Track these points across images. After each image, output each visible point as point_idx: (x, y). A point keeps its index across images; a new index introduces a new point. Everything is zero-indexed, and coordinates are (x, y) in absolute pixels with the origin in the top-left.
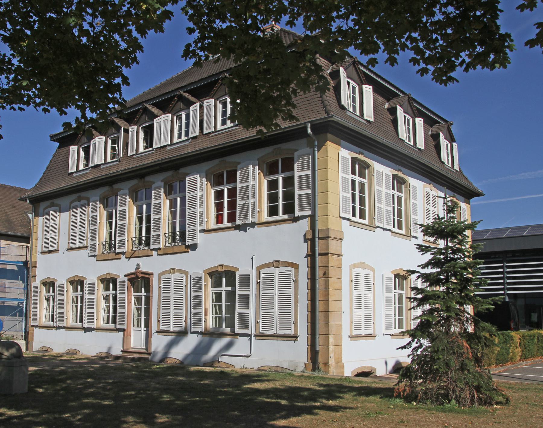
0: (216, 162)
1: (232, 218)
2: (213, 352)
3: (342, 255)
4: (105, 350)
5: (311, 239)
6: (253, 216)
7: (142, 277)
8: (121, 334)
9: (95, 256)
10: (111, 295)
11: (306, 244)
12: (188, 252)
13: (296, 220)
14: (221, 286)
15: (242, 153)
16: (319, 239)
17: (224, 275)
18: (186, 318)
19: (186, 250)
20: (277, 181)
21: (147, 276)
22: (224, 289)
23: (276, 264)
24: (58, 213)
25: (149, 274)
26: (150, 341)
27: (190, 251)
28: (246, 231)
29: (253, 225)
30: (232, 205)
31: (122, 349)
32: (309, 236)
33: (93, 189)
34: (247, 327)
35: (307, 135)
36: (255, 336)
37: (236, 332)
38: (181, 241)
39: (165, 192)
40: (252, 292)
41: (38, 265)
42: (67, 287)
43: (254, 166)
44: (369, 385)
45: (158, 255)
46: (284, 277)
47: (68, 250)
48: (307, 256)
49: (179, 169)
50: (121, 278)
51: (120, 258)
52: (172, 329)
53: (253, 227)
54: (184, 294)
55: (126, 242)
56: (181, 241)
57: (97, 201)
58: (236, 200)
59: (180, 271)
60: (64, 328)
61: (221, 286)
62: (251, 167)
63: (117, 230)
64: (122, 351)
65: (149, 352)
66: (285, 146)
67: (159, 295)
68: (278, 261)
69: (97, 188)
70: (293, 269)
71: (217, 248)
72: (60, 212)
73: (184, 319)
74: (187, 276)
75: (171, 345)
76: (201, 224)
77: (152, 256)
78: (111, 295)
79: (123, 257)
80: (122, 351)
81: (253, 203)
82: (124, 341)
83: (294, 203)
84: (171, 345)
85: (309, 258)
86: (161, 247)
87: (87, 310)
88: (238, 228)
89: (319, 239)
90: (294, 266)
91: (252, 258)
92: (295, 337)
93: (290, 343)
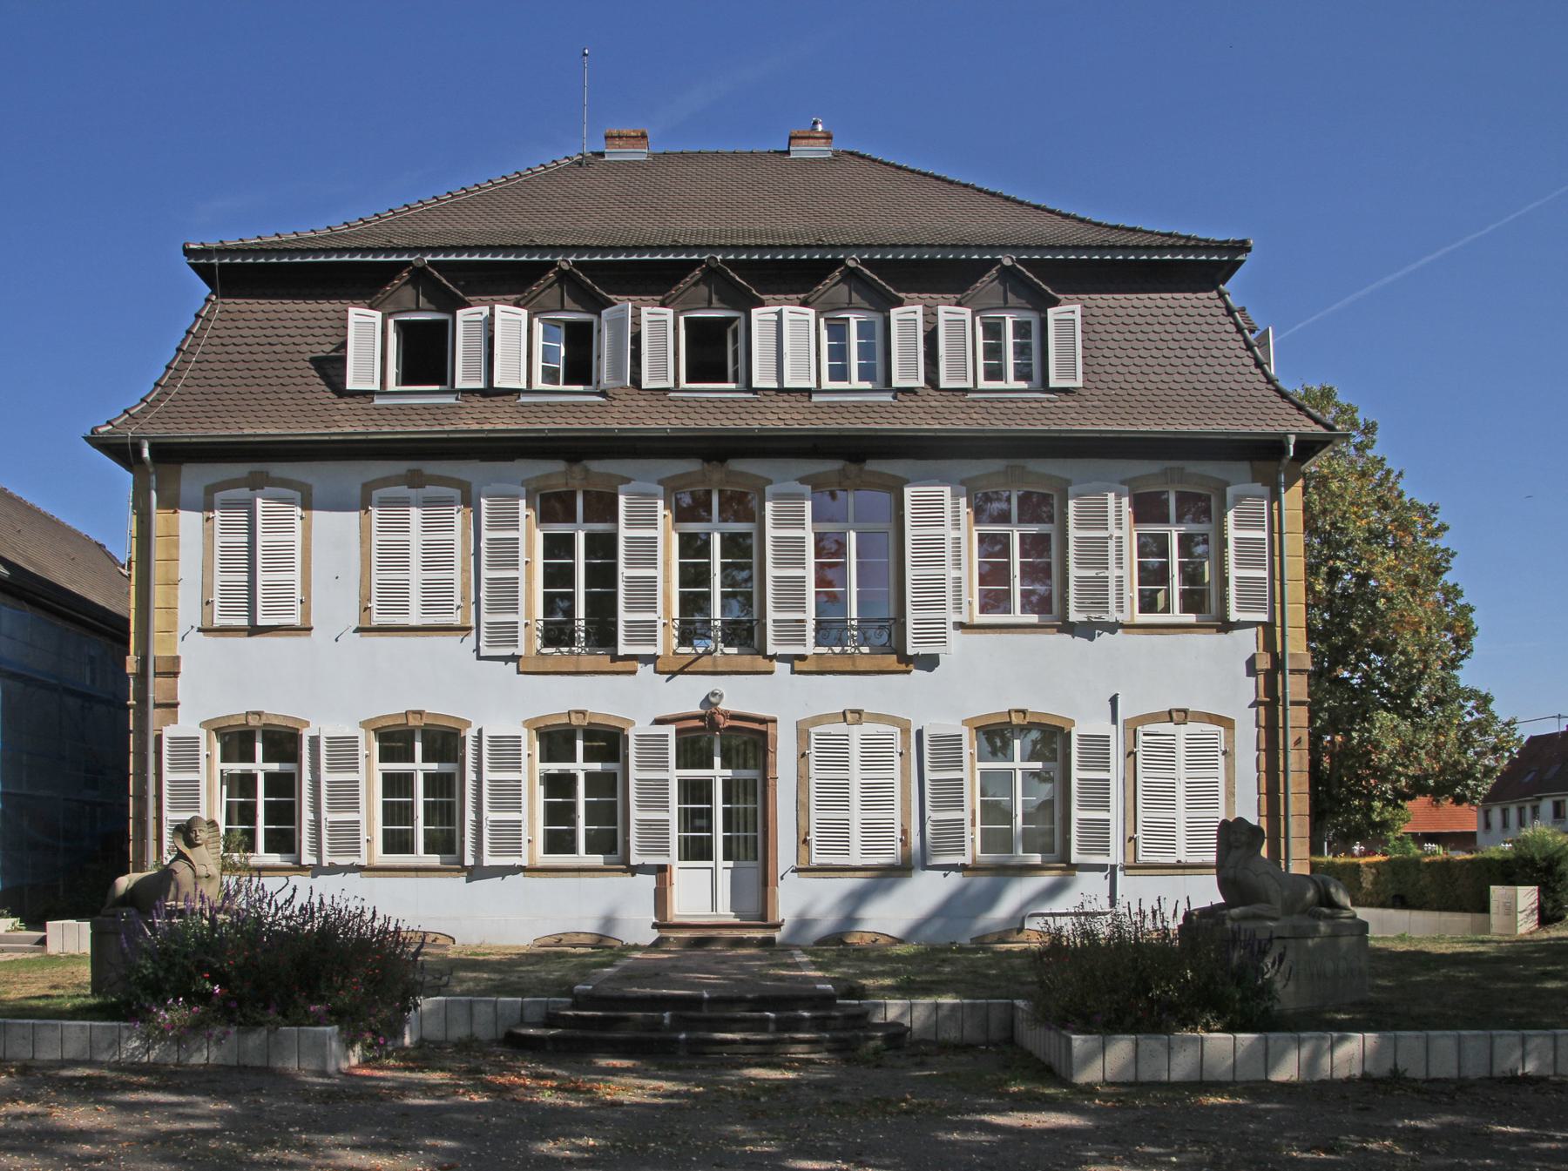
0: (997, 465)
1: (1192, 601)
2: (1005, 908)
3: (176, 705)
4: (590, 926)
5: (1267, 671)
6: (1120, 608)
7: (730, 728)
8: (650, 881)
9: (514, 658)
10: (1019, 773)
11: (1253, 679)
12: (908, 672)
13: (1226, 626)
14: (253, 760)
16: (156, 674)
18: (904, 832)
19: (903, 667)
20: (570, 539)
21: (762, 728)
22: (419, 767)
23: (1180, 716)
24: (298, 511)
25: (763, 721)
26: (774, 892)
27: (915, 672)
28: (1091, 639)
29: (1113, 628)
30: (603, 575)
32: (1264, 663)
33: (483, 459)
34: (1105, 850)
36: (1125, 868)
38: (890, 644)
40: (1115, 774)
41: (182, 669)
42: (209, 746)
43: (1119, 496)
44: (1420, 947)
45: (793, 672)
47: (358, 630)
48: (1256, 704)
49: (864, 461)
50: (639, 727)
51: (634, 673)
52: (856, 859)
54: (896, 774)
55: (660, 628)
56: (890, 644)
57: (517, 497)
58: (614, 567)
59: (878, 718)
60: (522, 869)
61: (253, 760)
62: (1111, 496)
63: (483, 595)
65: (770, 922)
66: (596, 466)
67: (802, 779)
68: (1185, 711)
69: (512, 459)
71: (983, 670)
72: (304, 508)
73: (898, 835)
74: (905, 731)
75: (859, 898)
76: (958, 608)
77: (771, 673)
78: (1019, 773)
79: (645, 671)
80: (655, 926)
81: (1120, 579)
82: (661, 898)
83: (614, 596)
84: (859, 898)
85: (1262, 709)
86: (660, 652)
87: (522, 817)
88: (1068, 628)
89: (156, 674)
90: (1227, 723)
91: (1114, 701)
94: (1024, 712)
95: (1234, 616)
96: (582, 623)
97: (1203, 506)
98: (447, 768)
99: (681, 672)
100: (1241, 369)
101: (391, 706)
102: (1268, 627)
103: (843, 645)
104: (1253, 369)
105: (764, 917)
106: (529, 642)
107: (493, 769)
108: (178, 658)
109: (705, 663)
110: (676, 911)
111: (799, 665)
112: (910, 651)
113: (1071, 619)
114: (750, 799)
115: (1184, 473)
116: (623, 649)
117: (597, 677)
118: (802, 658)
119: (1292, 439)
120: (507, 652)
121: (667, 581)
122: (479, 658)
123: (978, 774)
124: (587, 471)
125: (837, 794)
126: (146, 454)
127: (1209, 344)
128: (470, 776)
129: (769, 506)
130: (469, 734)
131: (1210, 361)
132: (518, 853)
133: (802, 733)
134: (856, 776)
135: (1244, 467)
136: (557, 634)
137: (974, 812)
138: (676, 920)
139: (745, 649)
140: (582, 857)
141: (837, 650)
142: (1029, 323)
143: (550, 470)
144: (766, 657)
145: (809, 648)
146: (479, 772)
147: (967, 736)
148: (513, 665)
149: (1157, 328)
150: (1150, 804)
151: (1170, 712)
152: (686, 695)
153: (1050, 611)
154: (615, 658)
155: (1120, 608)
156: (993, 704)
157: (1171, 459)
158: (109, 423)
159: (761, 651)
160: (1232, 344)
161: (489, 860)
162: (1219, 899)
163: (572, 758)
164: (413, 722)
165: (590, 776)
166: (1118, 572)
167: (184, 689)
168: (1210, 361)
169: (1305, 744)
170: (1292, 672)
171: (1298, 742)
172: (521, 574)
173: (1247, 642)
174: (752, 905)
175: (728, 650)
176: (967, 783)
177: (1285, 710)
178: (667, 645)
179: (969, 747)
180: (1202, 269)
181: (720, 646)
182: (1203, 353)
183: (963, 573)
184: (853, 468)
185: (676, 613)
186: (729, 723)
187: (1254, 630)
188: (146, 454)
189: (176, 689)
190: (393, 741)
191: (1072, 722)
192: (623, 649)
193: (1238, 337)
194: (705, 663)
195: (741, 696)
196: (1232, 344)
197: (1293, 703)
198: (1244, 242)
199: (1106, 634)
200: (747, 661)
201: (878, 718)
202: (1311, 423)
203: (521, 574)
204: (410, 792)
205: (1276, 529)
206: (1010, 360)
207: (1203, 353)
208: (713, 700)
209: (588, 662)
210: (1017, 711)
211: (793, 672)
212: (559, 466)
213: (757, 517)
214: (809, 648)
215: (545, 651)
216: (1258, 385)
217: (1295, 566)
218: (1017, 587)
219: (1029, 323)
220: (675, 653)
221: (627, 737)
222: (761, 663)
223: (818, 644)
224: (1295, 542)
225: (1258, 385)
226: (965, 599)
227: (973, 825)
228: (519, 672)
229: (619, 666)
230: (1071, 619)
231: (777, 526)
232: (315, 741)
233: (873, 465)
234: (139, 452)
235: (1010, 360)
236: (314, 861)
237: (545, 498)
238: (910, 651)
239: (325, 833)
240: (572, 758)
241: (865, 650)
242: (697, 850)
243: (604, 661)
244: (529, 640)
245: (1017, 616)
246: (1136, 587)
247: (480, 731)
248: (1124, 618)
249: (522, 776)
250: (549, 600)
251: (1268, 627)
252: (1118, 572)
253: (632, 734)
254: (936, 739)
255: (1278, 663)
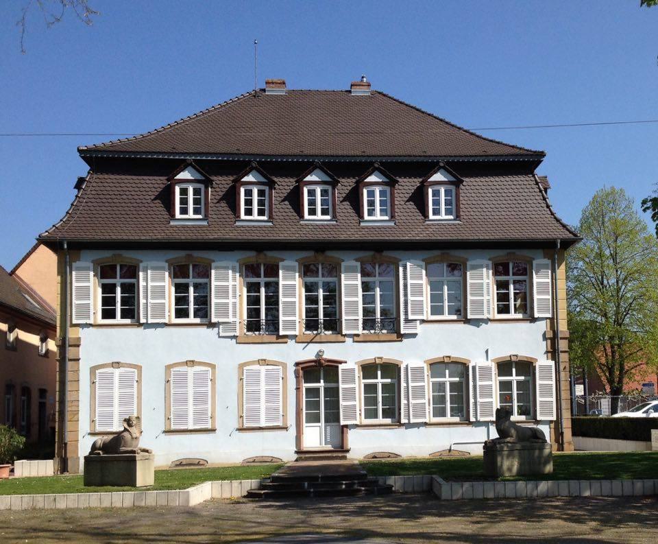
3: (78, 360)
6: (489, 313)
9: (235, 337)
13: (533, 320)
15: (472, 250)
17: (514, 365)
31: (296, 450)
32: (550, 335)
33: (220, 250)
35: (63, 248)
37: (538, 419)
39: (170, 276)
45: (354, 342)
46: (200, 379)
49: (382, 251)
51: (286, 343)
53: (487, 323)
59: (200, 364)
64: (296, 452)
66: (270, 254)
70: (136, 371)
77: (344, 342)
78: (515, 382)
80: (296, 452)
81: (488, 301)
91: (487, 352)
92: (286, 428)
93: (284, 432)
94: (449, 357)
95: (536, 315)
96: (264, 321)
97: (525, 271)
98: (332, 385)
99: (311, 342)
100: (541, 209)
101: (504, 352)
102: (552, 319)
103: (259, 331)
104: (545, 208)
105: (342, 447)
106: (241, 330)
107: (413, 381)
108: (80, 338)
109: (317, 339)
110: (304, 446)
111: (356, 339)
112: (402, 332)
113: (468, 318)
114: (392, 393)
115: (515, 257)
116: (282, 333)
117: (270, 345)
118: (358, 335)
119: (559, 241)
120: (232, 334)
121: (300, 303)
122: (219, 337)
123: (431, 383)
124: (265, 255)
125: (271, 395)
126: (66, 247)
127: (527, 198)
128: (403, 384)
129: (213, 272)
130: (403, 367)
131: (527, 205)
132: (355, 419)
133: (93, 370)
134: (116, 392)
135: (540, 252)
136: (253, 326)
137: (429, 400)
138: (305, 449)
139: (334, 332)
140: (381, 420)
141: (372, 331)
142: (200, 189)
143: (250, 256)
144: (342, 335)
145: (360, 331)
146: (407, 383)
147: (426, 366)
148: (234, 341)
149: (506, 191)
150: (102, 405)
151: (187, 362)
152: (308, 353)
153: (461, 314)
154: (279, 337)
155: (489, 313)
156: (437, 354)
157: (509, 249)
158: (46, 232)
159: (340, 332)
160: (537, 198)
161: (412, 421)
162: (498, 436)
163: (511, 375)
164: (378, 361)
165: (384, 385)
166: (488, 298)
167: (82, 352)
168: (527, 205)
169: (568, 369)
170: (561, 338)
171: (565, 368)
172: (91, 302)
173: (543, 326)
174: (337, 441)
175: (327, 332)
176: (426, 387)
177: (558, 355)
178: (300, 330)
179: (427, 372)
180: (523, 163)
181: (323, 330)
182: (525, 202)
183: (490, 298)
184: (378, 255)
185: (304, 317)
186: (327, 364)
187: (544, 322)
188: (66, 247)
189: (79, 352)
190: (504, 367)
191: (536, 360)
192: (282, 333)
193: (540, 194)
194: (317, 339)
195: (331, 352)
196: (537, 198)
197: (562, 352)
198: (542, 152)
199: (484, 324)
200: (334, 337)
201: (200, 364)
202: (568, 233)
203: (91, 302)
204: (376, 392)
205: (554, 279)
206: (443, 207)
207: (525, 202)
208: (320, 354)
209: (267, 338)
210: (447, 357)
211: (354, 342)
212: (253, 254)
213: (208, 276)
214: (360, 331)
215: (247, 333)
216: (547, 216)
217: (562, 294)
218: (446, 304)
219: (200, 189)
220: (245, 334)
221: (534, 368)
222: (341, 339)
223: (364, 329)
224: (562, 285)
225: (547, 216)
226: (491, 306)
227: (429, 405)
228: (237, 343)
229: (280, 340)
230: (468, 318)
231: (284, 279)
232: (474, 368)
233: (386, 253)
234: (63, 245)
235: (443, 207)
236: (406, 421)
237: (102, 268)
238: (402, 332)
239: (478, 407)
240: (511, 375)
241: (384, 331)
242: (314, 418)
243: (273, 338)
244: (241, 328)
245: (446, 317)
246: (496, 303)
247: (407, 366)
248: (491, 317)
249: (425, 384)
250: (308, 311)
251: (552, 319)
252: (488, 298)
253: (537, 365)
254: (413, 369)
255: (555, 333)
